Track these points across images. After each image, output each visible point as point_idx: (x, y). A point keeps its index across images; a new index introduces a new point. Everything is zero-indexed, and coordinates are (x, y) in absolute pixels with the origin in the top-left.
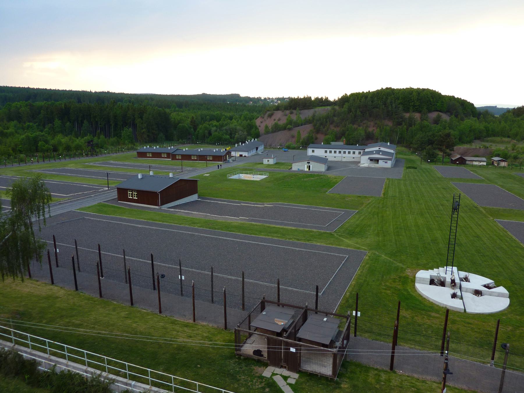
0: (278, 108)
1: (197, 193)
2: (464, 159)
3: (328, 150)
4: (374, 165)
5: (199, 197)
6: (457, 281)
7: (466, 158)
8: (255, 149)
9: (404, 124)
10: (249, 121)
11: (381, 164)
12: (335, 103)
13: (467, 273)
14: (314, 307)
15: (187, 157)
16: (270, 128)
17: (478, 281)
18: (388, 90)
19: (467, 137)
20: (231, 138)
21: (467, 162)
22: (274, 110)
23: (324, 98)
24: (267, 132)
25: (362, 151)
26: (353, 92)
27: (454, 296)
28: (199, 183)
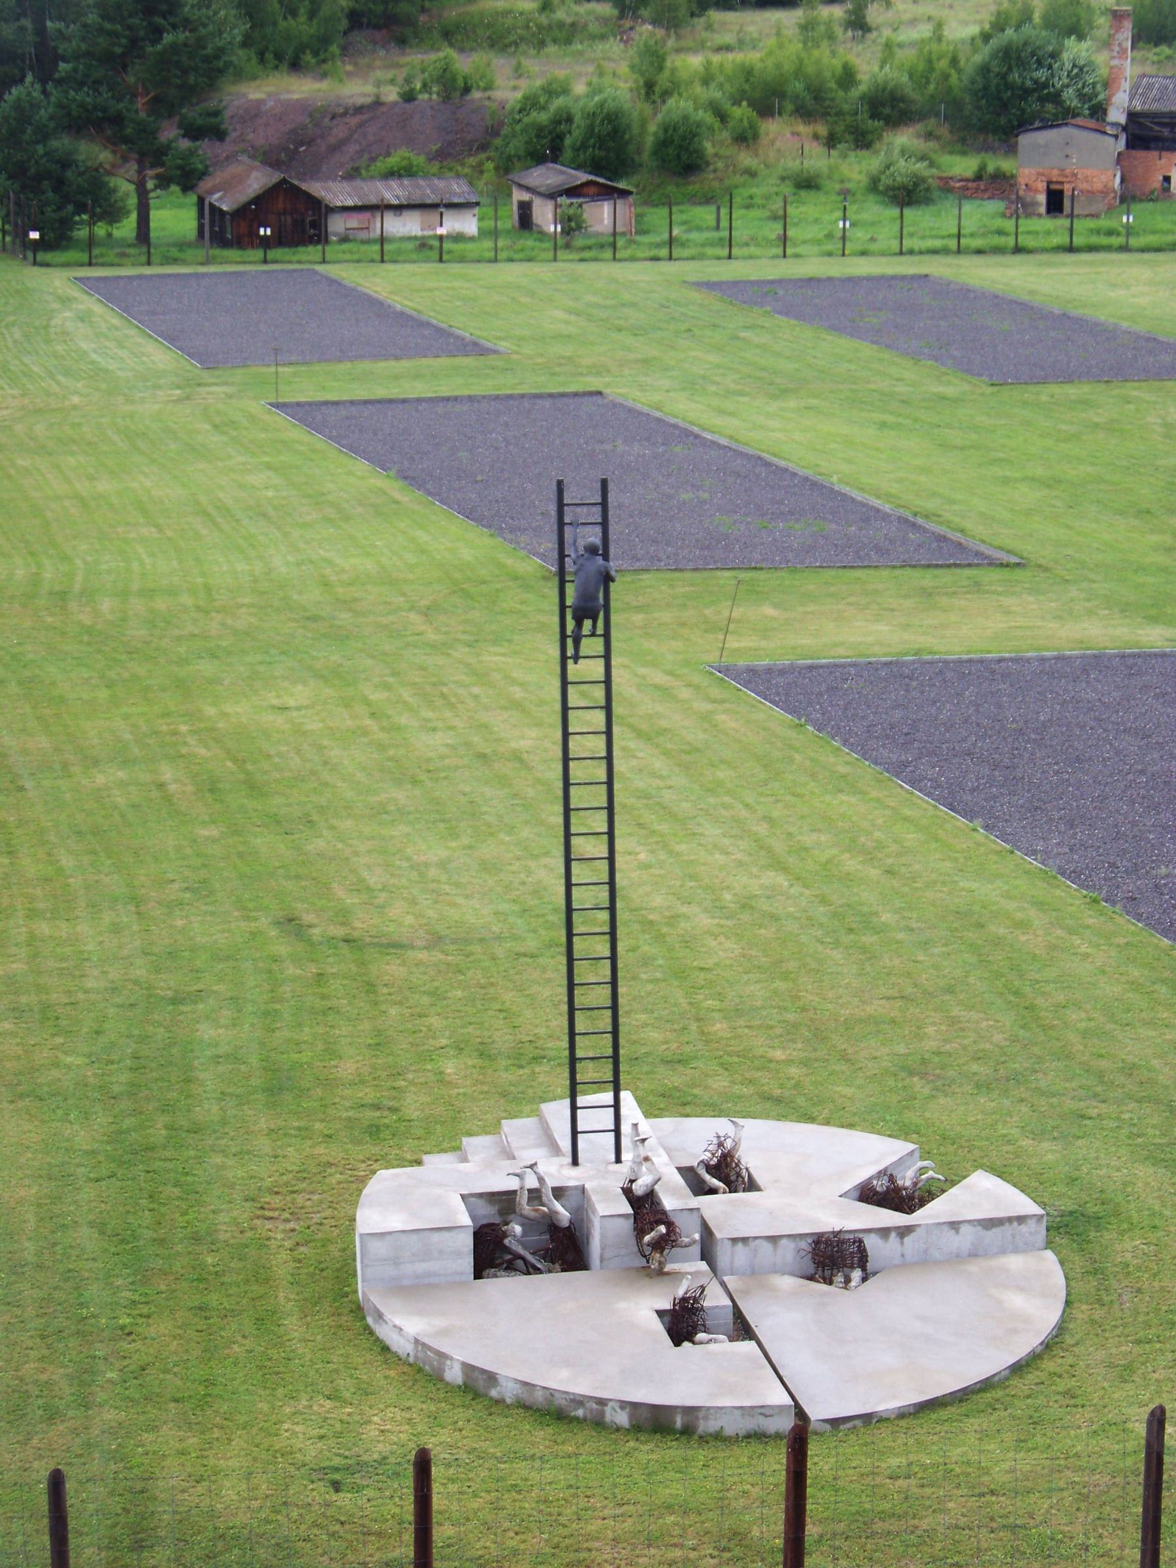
2: (309, 197)
6: (674, 1198)
7: (316, 188)
13: (722, 1126)
17: (809, 1173)
21: (337, 225)
27: (683, 1323)
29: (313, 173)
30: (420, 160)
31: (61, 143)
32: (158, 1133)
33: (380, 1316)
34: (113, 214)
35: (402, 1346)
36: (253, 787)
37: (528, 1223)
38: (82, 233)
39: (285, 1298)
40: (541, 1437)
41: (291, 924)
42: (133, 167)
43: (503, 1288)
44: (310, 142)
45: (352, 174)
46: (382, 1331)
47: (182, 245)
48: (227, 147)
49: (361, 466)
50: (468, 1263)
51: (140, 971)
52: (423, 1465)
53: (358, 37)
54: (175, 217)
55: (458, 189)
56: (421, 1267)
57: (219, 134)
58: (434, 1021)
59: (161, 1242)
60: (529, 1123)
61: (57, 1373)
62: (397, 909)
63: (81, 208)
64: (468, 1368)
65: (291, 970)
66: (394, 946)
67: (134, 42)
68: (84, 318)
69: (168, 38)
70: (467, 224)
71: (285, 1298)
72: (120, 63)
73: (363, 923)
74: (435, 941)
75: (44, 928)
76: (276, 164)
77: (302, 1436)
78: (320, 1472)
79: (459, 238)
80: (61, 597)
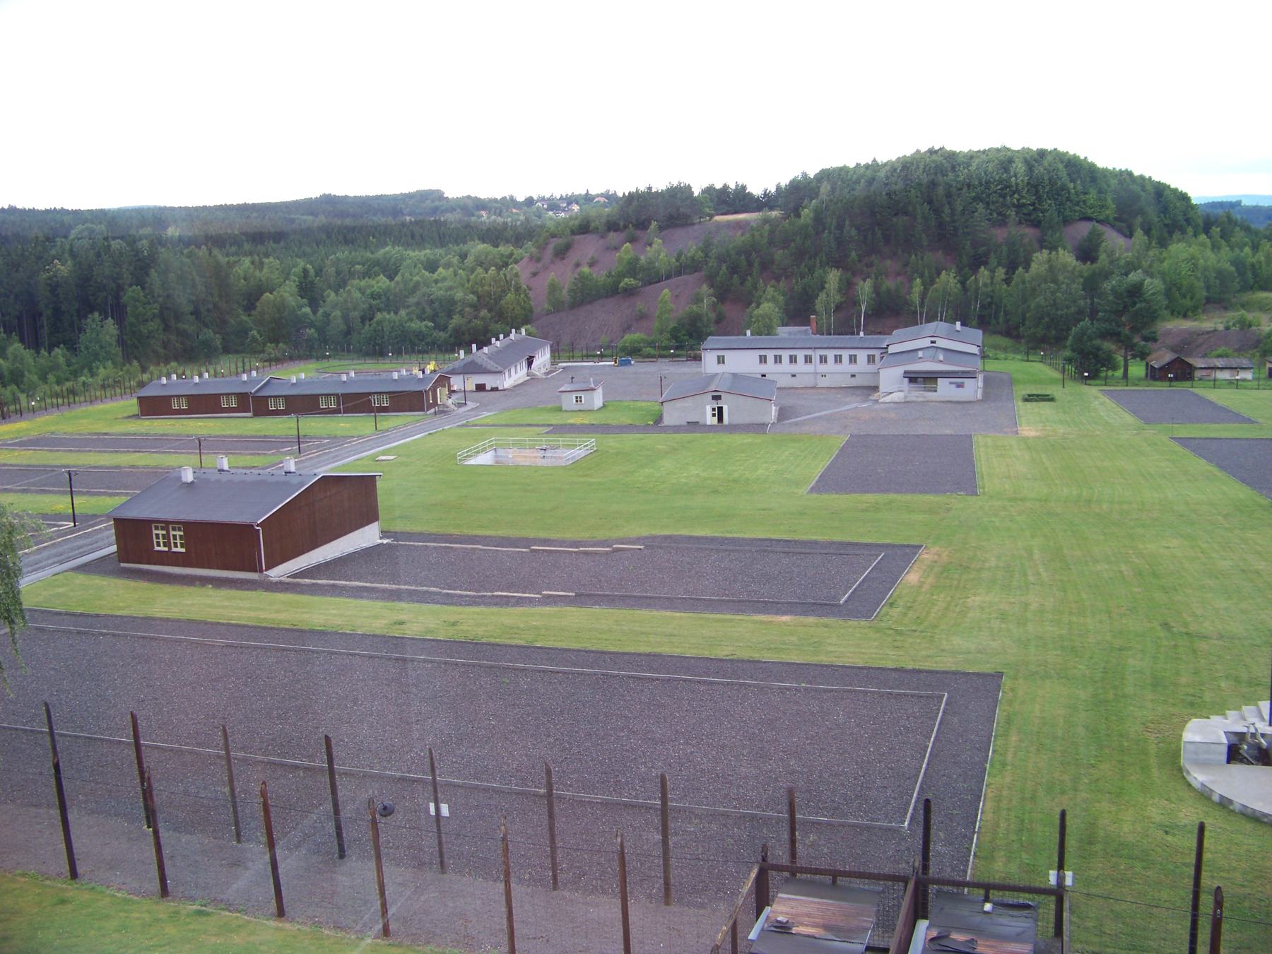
0: (584, 228)
1: (376, 519)
2: (1190, 366)
3: (770, 355)
4: (918, 394)
5: (384, 534)
7: (1190, 360)
8: (525, 364)
9: (993, 261)
10: (492, 270)
11: (945, 388)
12: (766, 202)
14: (785, 860)
15: (303, 404)
16: (565, 292)
18: (934, 157)
19: (1184, 296)
20: (438, 327)
21: (1198, 374)
22: (573, 233)
23: (733, 186)
24: (558, 307)
25: (877, 353)
26: (827, 166)
28: (379, 484)
29: (1190, 355)
30: (1230, 351)
31: (1097, 342)
32: (1111, 696)
33: (1188, 773)
34: (1114, 368)
35: (1195, 784)
36: (1155, 575)
37: (1249, 745)
38: (1103, 374)
39: (1153, 761)
40: (1249, 826)
41: (1166, 625)
42: (1123, 351)
43: (1236, 768)
44: (1189, 344)
45: (1205, 356)
46: (1189, 778)
47: (1140, 379)
48: (1158, 344)
49: (1203, 462)
50: (1224, 757)
51: (1108, 638)
52: (1202, 828)
53: (1208, 306)
54: (1137, 370)
55: (1245, 362)
56: (1206, 756)
57: (1155, 340)
58: (1218, 666)
59: (1108, 735)
60: (1253, 708)
61: (1066, 777)
62: (1206, 624)
63: (1103, 365)
64: (1222, 797)
65: (1165, 643)
66: (1204, 637)
67: (1125, 307)
68: (1102, 404)
69: (1138, 306)
70: (1248, 375)
71: (1153, 761)
72: (1119, 313)
73: (1193, 628)
74: (1221, 637)
75: (1074, 619)
76: (1175, 352)
77: (1155, 812)
78: (1161, 826)
79: (1244, 380)
80: (1089, 502)
